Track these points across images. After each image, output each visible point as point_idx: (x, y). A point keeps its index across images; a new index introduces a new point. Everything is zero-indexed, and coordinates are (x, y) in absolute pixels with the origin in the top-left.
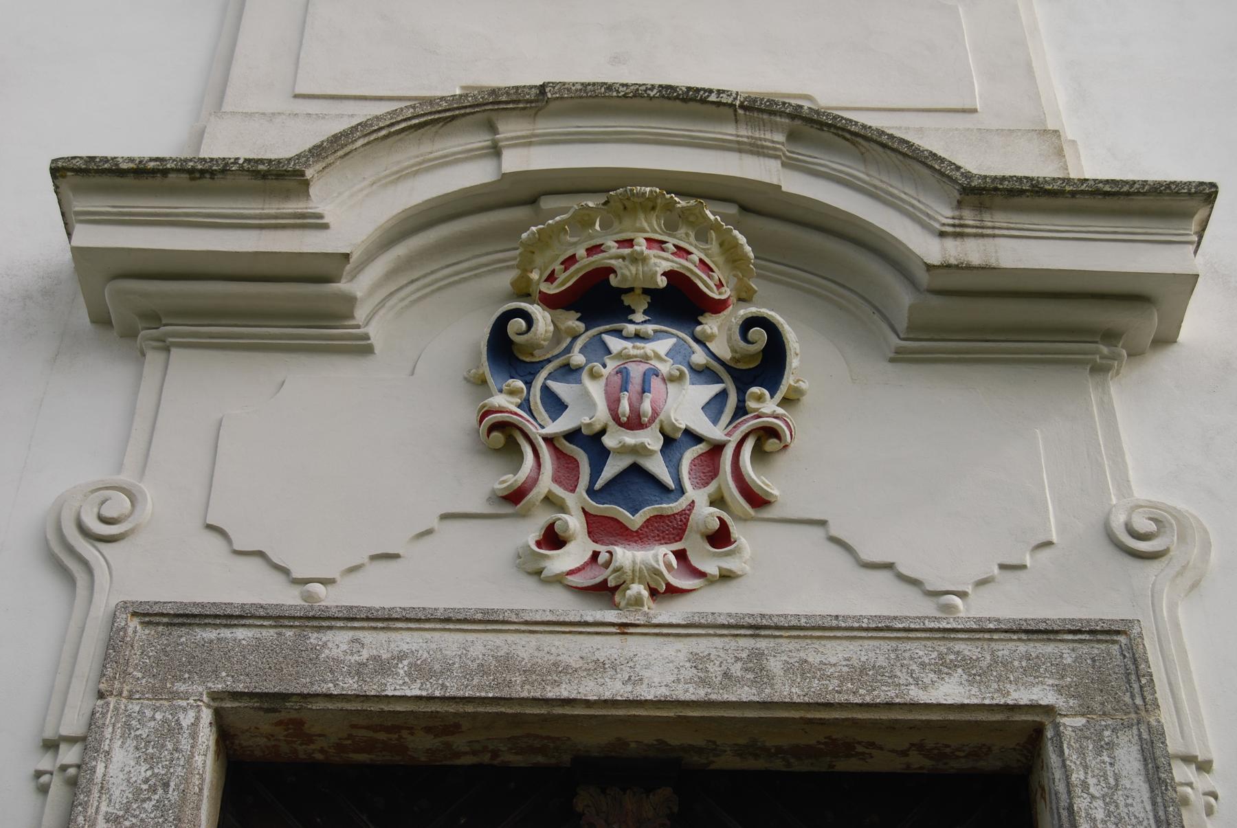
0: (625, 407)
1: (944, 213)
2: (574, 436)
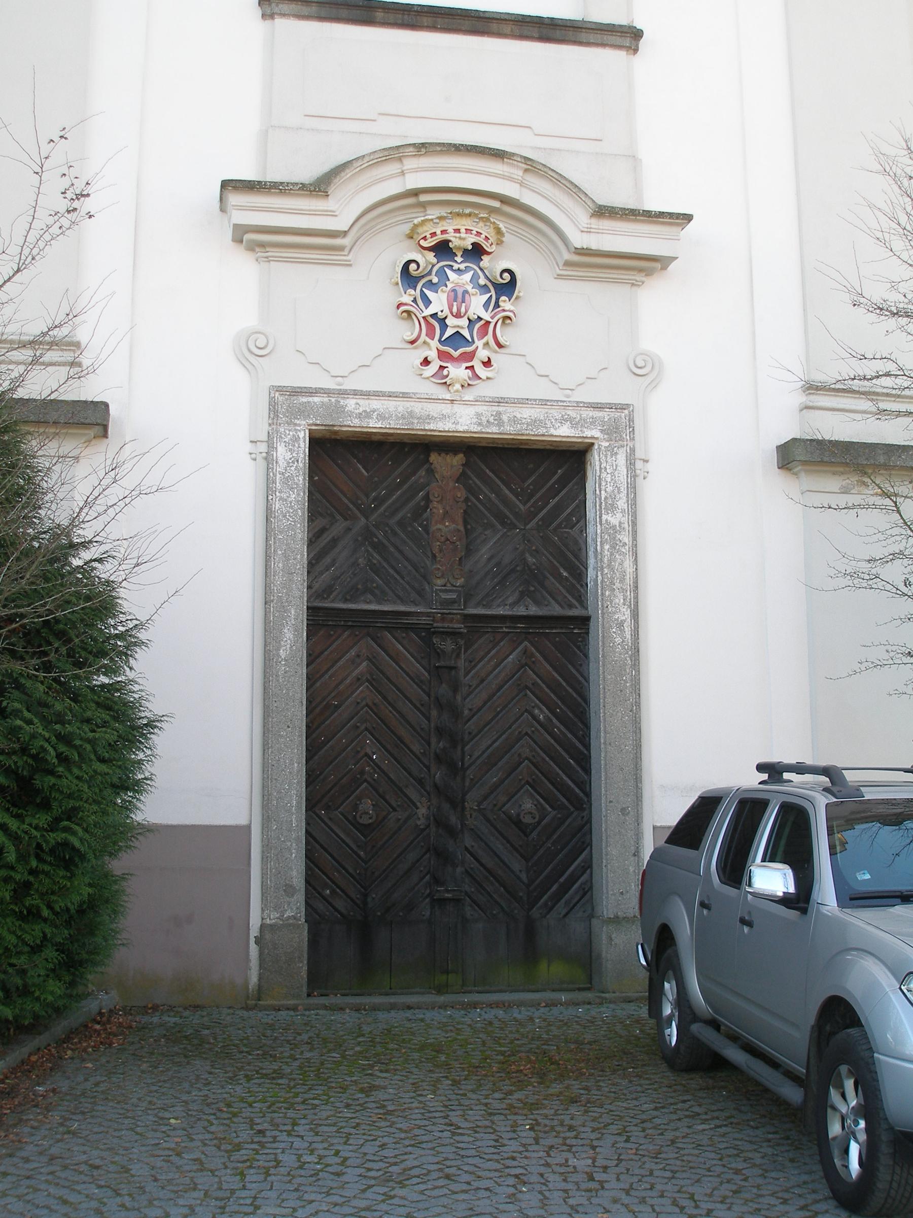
0: (455, 310)
1: (584, 218)
2: (434, 316)
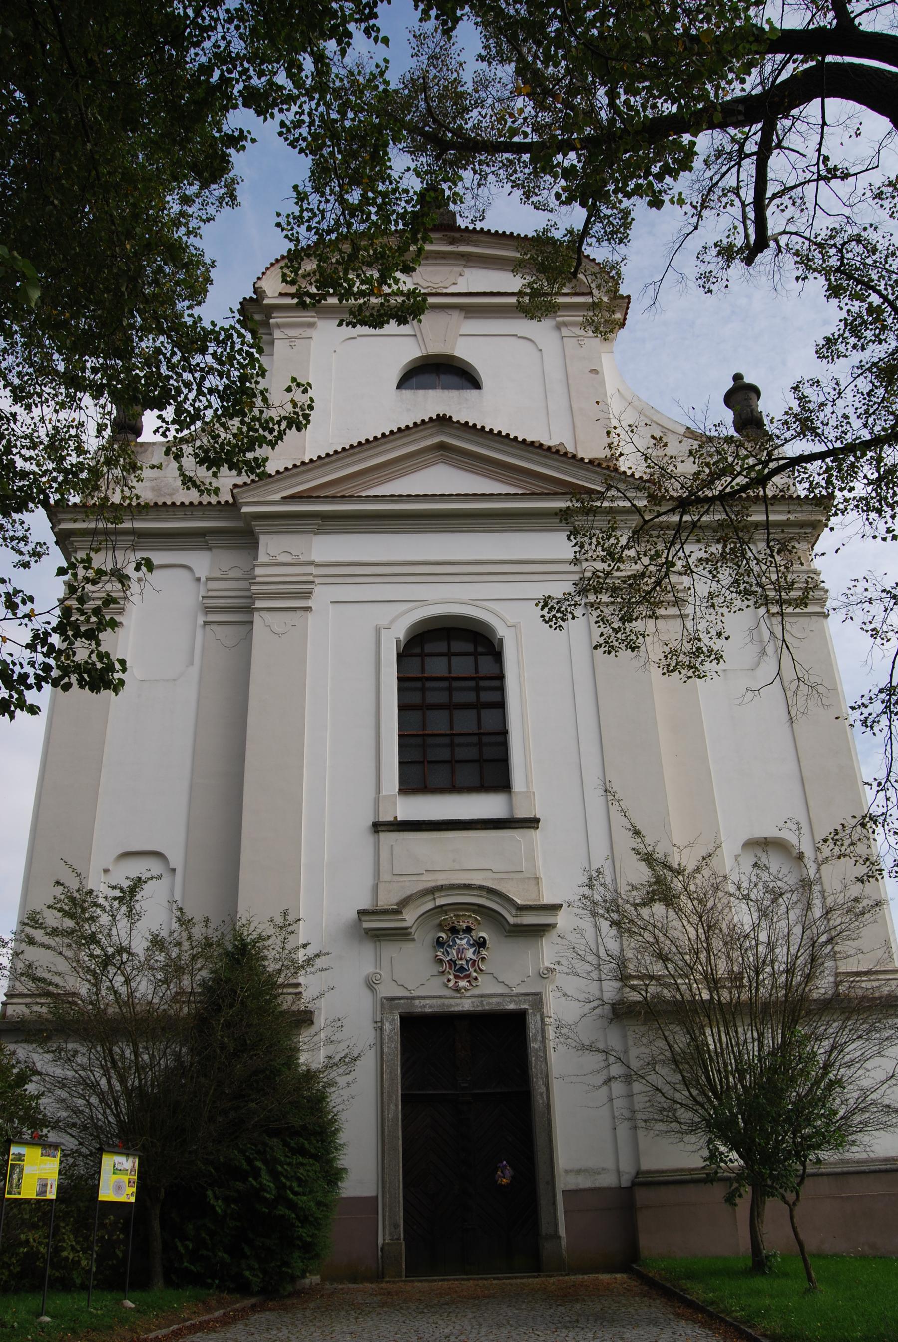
1: (514, 912)
